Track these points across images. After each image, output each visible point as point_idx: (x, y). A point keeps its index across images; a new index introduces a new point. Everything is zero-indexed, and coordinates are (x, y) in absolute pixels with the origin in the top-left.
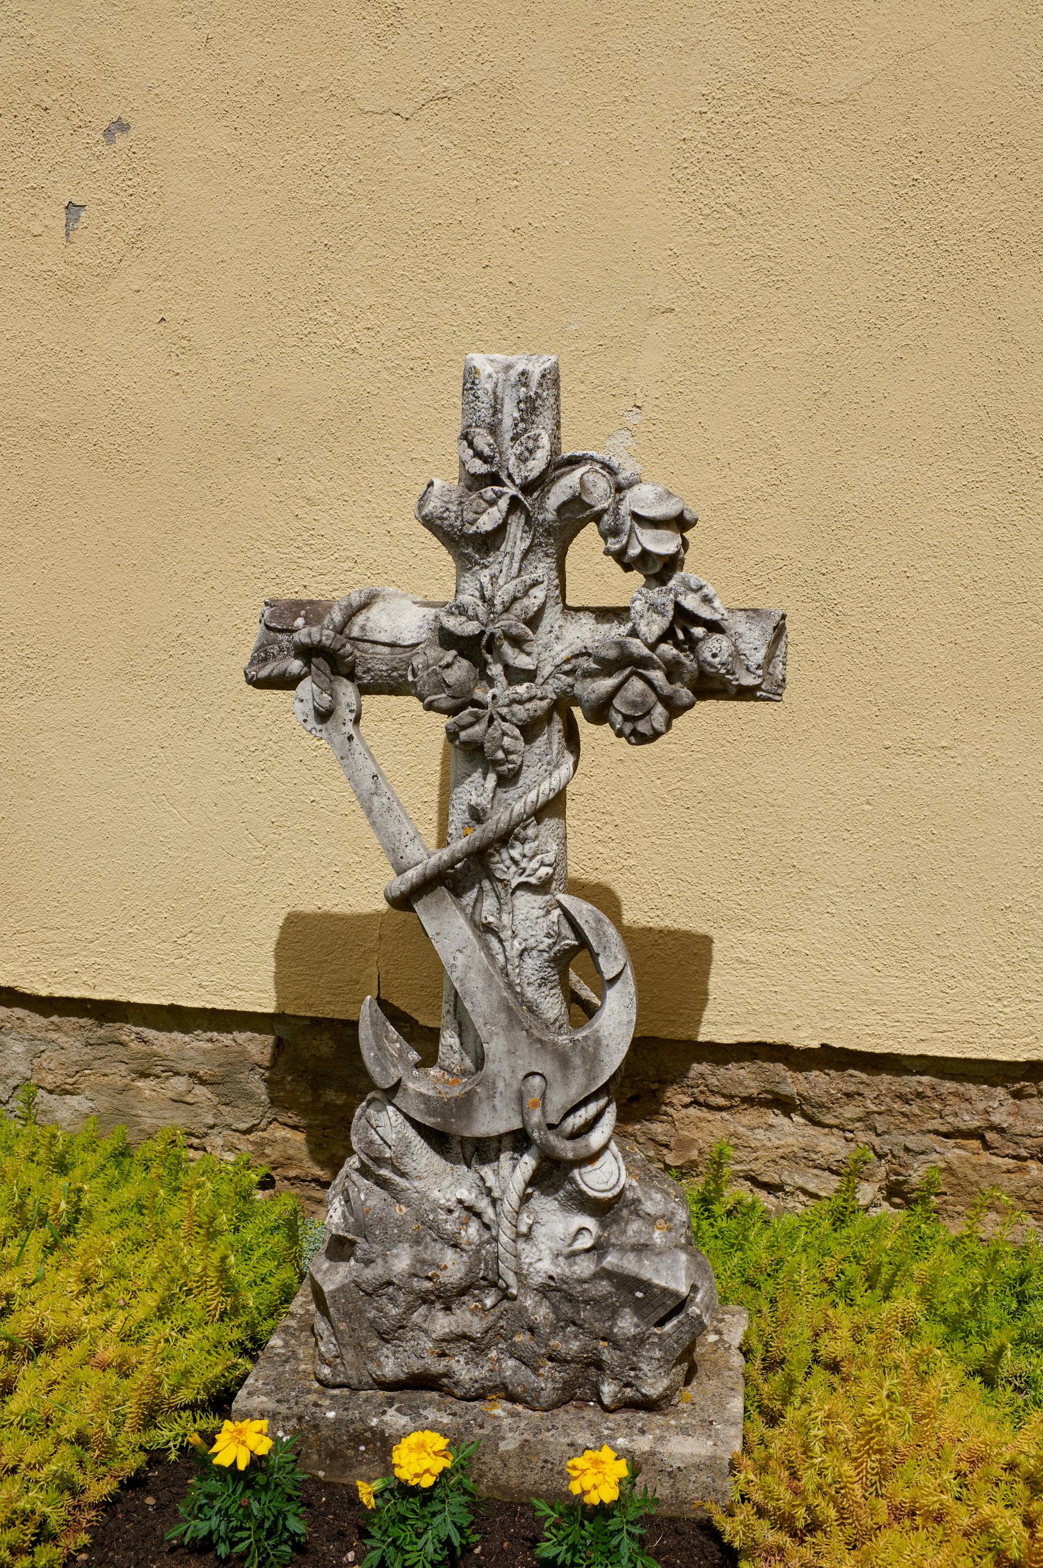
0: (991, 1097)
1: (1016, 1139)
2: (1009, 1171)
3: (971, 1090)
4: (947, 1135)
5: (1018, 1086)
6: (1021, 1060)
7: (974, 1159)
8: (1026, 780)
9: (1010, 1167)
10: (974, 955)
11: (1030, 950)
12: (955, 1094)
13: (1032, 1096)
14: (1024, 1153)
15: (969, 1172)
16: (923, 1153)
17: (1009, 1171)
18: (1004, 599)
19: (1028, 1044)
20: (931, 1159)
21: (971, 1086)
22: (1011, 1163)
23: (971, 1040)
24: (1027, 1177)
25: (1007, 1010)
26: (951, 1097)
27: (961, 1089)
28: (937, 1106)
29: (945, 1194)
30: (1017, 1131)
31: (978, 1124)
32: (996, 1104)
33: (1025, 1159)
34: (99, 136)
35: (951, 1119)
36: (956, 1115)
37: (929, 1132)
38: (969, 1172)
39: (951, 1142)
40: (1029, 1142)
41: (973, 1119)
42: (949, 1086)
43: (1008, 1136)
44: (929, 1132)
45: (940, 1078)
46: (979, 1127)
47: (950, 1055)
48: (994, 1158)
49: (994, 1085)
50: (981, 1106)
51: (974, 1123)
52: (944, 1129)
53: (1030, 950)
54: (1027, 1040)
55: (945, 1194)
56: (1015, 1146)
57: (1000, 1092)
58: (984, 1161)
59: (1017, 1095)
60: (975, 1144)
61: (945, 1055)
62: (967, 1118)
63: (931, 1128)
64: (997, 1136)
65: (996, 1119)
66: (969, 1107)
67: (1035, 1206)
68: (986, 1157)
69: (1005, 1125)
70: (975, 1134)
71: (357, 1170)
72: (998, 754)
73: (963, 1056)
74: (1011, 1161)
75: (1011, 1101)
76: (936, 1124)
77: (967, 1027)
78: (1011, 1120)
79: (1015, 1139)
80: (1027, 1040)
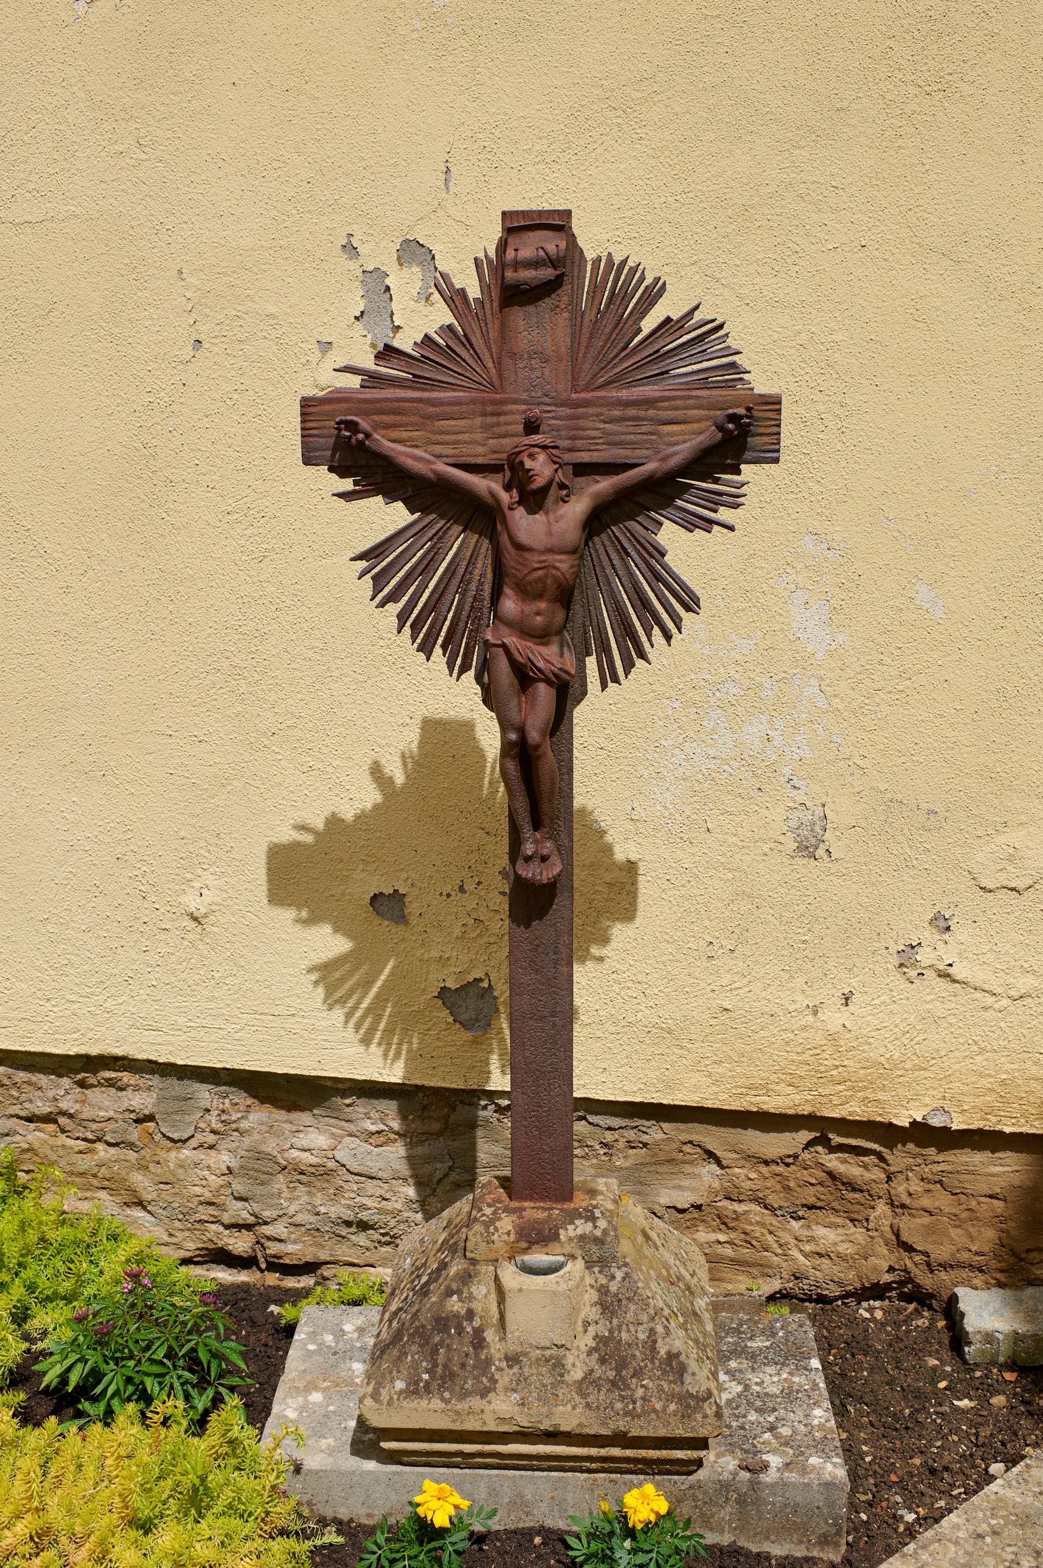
0: (58, 1086)
1: (84, 1123)
2: (81, 1152)
3: (42, 1079)
4: (29, 1120)
5: (79, 1077)
6: (71, 1053)
7: (52, 1141)
8: (49, 808)
9: (81, 1148)
10: (23, 961)
11: (69, 957)
12: (29, 1083)
13: (92, 1086)
14: (90, 1136)
15: (49, 1152)
16: (7, 1135)
17: (81, 1152)
18: (16, 651)
19: (76, 1040)
20: (15, 1140)
21: (41, 1076)
22: (82, 1145)
23: (29, 1035)
24: (96, 1157)
25: (55, 1009)
26: (25, 1086)
27: (34, 1079)
28: (15, 1094)
29: (33, 1171)
30: (84, 1117)
31: (49, 1110)
32: (62, 1093)
33: (93, 1142)
34: (460, 895)
35: (27, 1105)
36: (31, 1101)
37: (12, 1116)
38: (49, 1152)
39: (32, 1126)
40: (94, 1126)
41: (44, 1105)
42: (22, 1076)
43: (77, 1121)
44: (12, 1116)
45: (15, 1069)
46: (51, 1113)
47: (13, 1048)
48: (68, 1140)
49: (60, 1076)
50: (51, 1094)
51: (47, 1109)
52: (23, 1114)
53: (69, 957)
54: (75, 1036)
55: (33, 1171)
56: (83, 1130)
57: (66, 1082)
58: (60, 1143)
59: (82, 1084)
60: (51, 1127)
61: (9, 1048)
62: (40, 1104)
63: (12, 1113)
64: (68, 1121)
65: (64, 1105)
66: (41, 1094)
67: (107, 1183)
68: (63, 1139)
69: (72, 1111)
70: (48, 1119)
71: (1008, 1469)
72: (24, 784)
73: (24, 1050)
74: (83, 1143)
75: (78, 1090)
76: (16, 1110)
77: (24, 1023)
78: (78, 1106)
79: (83, 1123)
80: (75, 1036)
